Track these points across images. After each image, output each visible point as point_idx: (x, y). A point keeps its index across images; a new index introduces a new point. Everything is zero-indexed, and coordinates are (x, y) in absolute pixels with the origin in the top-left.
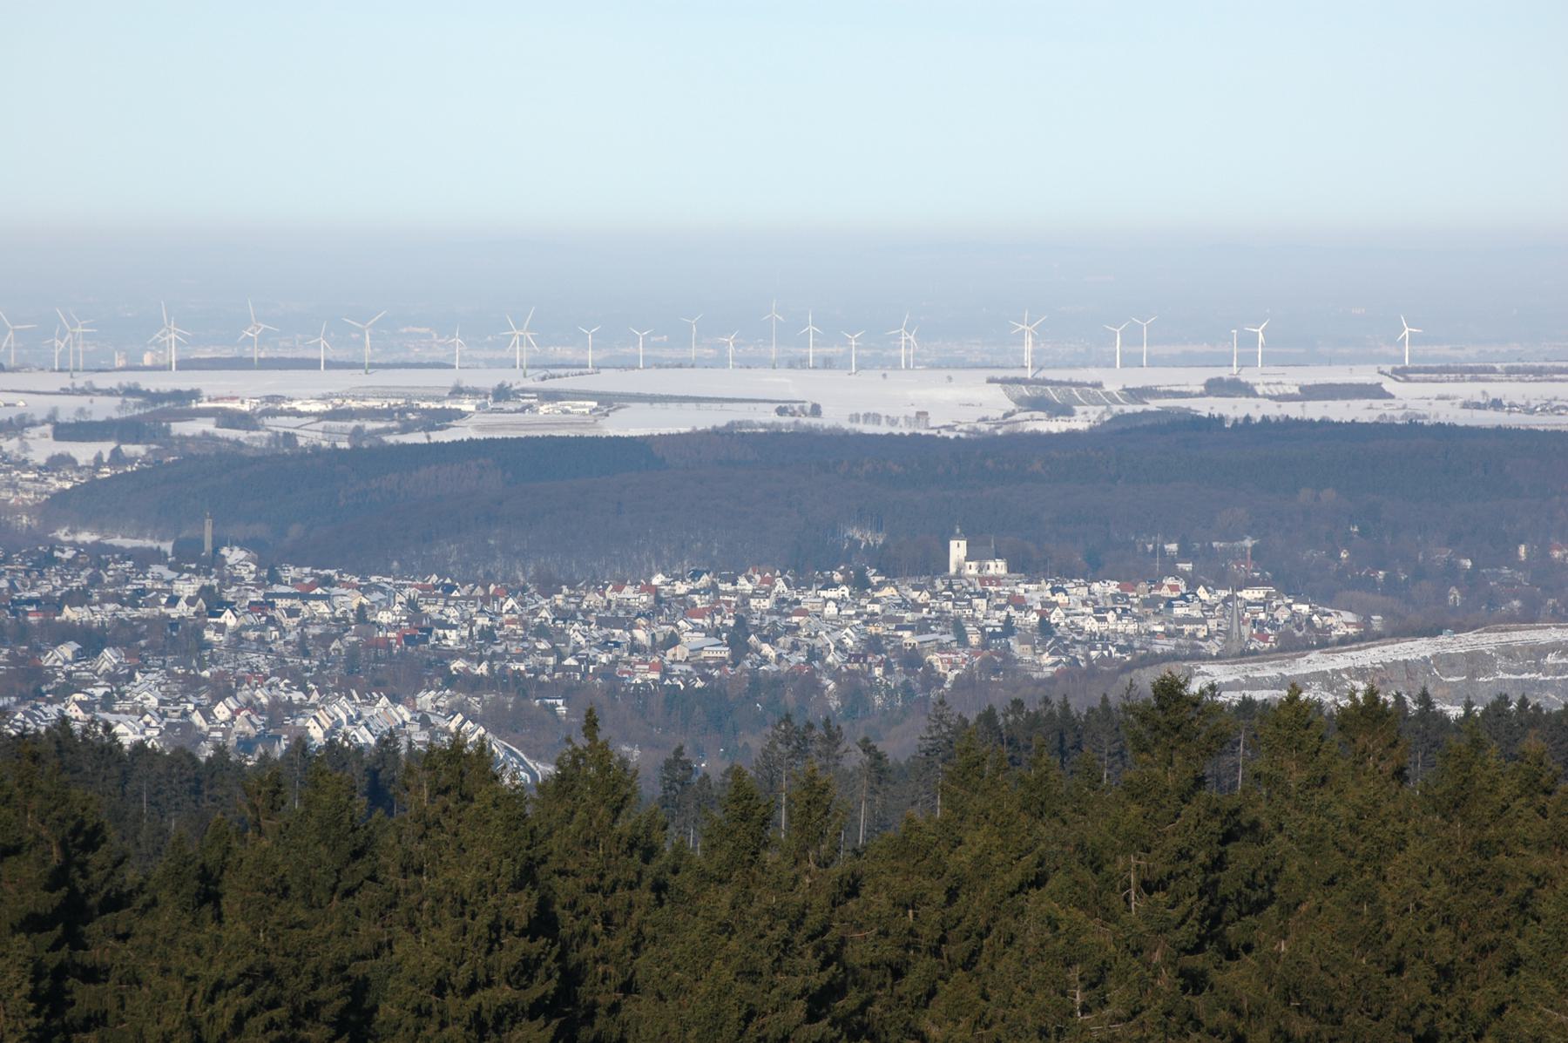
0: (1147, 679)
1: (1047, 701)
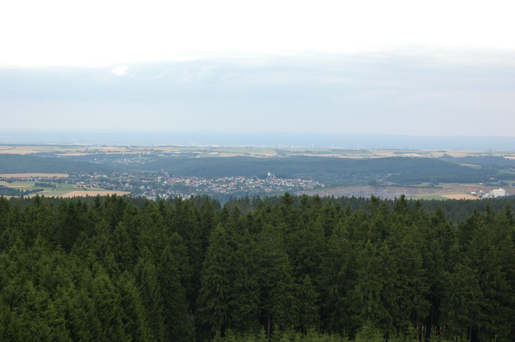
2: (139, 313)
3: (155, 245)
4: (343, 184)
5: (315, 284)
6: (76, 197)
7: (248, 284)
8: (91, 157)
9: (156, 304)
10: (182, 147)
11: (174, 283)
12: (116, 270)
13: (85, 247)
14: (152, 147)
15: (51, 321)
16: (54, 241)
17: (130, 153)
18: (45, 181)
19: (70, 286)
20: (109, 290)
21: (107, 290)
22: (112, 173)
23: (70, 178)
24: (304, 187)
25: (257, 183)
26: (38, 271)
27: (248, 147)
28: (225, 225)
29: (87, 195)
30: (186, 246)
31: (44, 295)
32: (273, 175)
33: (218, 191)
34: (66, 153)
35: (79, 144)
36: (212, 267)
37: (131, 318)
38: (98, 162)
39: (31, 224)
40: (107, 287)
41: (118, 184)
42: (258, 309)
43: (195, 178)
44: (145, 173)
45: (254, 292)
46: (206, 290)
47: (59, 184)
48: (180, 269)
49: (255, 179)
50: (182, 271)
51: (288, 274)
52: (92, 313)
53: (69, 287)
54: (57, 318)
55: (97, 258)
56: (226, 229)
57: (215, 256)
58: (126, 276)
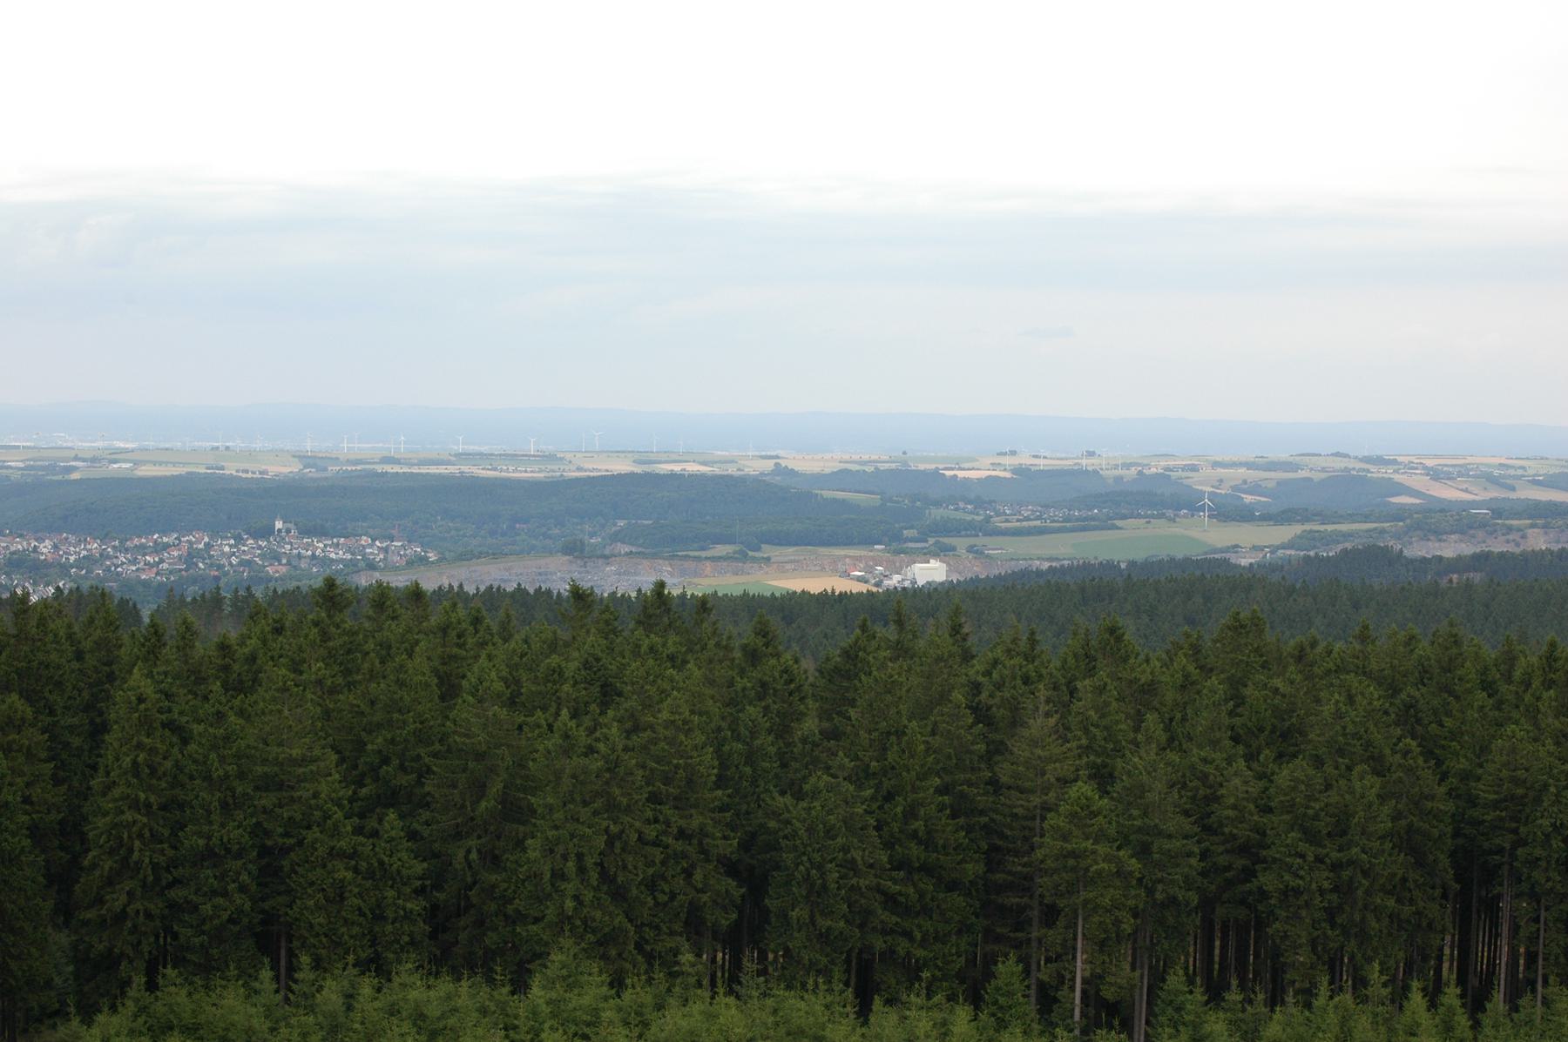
5: (413, 836)
10: (29, 448)
25: (244, 551)
27: (218, 448)
28: (155, 670)
33: (133, 575)
36: (116, 792)
43: (66, 539)
45: (239, 863)
46: (103, 857)
48: (27, 800)
49: (239, 539)
50: (32, 803)
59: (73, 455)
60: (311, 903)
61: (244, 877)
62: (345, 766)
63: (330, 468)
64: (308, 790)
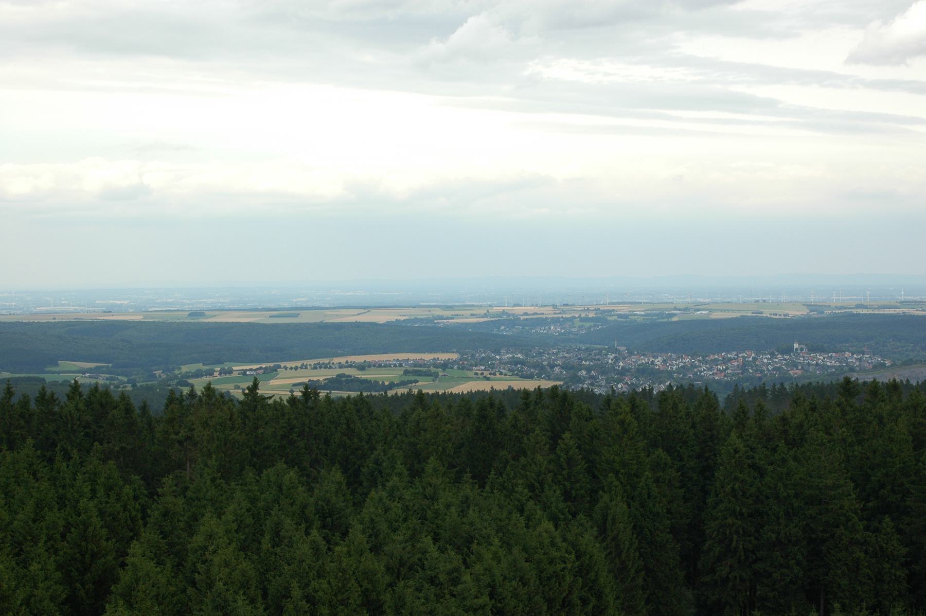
0: (841, 379)
1: (818, 383)
2: (606, 587)
3: (627, 470)
4: (923, 360)
5: (900, 531)
6: (473, 392)
7: (786, 534)
8: (497, 324)
9: (633, 571)
10: (647, 303)
11: (660, 534)
12: (563, 514)
13: (511, 476)
14: (596, 305)
15: (468, 603)
16: (456, 467)
17: (561, 316)
18: (420, 366)
19: (493, 543)
20: (558, 549)
21: (554, 549)
22: (531, 351)
23: (461, 361)
24: (855, 366)
25: (776, 362)
26: (436, 518)
27: (758, 301)
28: (744, 434)
29: (492, 388)
30: (677, 472)
31: (455, 559)
32: (803, 346)
33: (711, 377)
34: (453, 319)
35: (475, 304)
36: (722, 506)
37: (592, 596)
38: (507, 331)
39: (417, 439)
40: (553, 544)
41: (543, 368)
42: (804, 576)
43: (671, 356)
44: (587, 349)
45: (796, 548)
46: (714, 545)
47: (444, 370)
48: (669, 512)
49: (773, 355)
50: (671, 513)
51: (854, 515)
52: (533, 588)
53: (492, 544)
54: (476, 597)
55: (530, 494)
56: (745, 441)
57: (728, 488)
58: (582, 525)
59: (673, 307)
60: (839, 572)
61: (799, 557)
62: (858, 490)
63: (825, 312)
64: (837, 504)
